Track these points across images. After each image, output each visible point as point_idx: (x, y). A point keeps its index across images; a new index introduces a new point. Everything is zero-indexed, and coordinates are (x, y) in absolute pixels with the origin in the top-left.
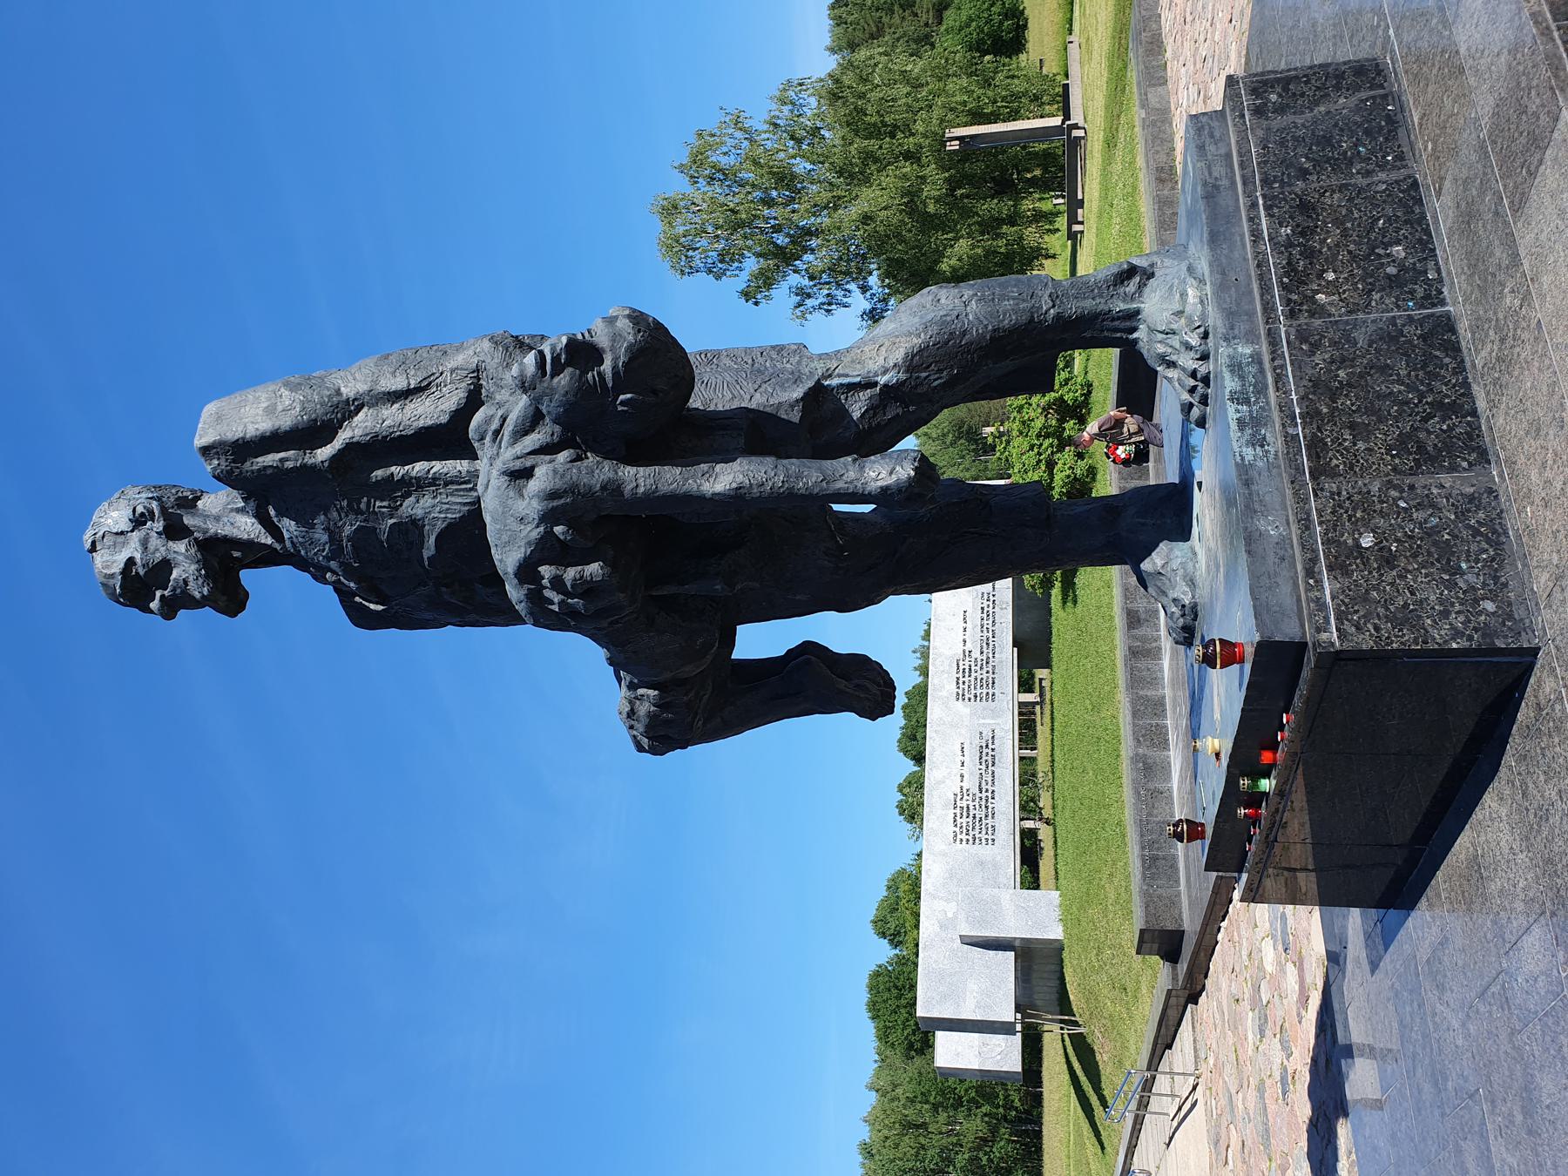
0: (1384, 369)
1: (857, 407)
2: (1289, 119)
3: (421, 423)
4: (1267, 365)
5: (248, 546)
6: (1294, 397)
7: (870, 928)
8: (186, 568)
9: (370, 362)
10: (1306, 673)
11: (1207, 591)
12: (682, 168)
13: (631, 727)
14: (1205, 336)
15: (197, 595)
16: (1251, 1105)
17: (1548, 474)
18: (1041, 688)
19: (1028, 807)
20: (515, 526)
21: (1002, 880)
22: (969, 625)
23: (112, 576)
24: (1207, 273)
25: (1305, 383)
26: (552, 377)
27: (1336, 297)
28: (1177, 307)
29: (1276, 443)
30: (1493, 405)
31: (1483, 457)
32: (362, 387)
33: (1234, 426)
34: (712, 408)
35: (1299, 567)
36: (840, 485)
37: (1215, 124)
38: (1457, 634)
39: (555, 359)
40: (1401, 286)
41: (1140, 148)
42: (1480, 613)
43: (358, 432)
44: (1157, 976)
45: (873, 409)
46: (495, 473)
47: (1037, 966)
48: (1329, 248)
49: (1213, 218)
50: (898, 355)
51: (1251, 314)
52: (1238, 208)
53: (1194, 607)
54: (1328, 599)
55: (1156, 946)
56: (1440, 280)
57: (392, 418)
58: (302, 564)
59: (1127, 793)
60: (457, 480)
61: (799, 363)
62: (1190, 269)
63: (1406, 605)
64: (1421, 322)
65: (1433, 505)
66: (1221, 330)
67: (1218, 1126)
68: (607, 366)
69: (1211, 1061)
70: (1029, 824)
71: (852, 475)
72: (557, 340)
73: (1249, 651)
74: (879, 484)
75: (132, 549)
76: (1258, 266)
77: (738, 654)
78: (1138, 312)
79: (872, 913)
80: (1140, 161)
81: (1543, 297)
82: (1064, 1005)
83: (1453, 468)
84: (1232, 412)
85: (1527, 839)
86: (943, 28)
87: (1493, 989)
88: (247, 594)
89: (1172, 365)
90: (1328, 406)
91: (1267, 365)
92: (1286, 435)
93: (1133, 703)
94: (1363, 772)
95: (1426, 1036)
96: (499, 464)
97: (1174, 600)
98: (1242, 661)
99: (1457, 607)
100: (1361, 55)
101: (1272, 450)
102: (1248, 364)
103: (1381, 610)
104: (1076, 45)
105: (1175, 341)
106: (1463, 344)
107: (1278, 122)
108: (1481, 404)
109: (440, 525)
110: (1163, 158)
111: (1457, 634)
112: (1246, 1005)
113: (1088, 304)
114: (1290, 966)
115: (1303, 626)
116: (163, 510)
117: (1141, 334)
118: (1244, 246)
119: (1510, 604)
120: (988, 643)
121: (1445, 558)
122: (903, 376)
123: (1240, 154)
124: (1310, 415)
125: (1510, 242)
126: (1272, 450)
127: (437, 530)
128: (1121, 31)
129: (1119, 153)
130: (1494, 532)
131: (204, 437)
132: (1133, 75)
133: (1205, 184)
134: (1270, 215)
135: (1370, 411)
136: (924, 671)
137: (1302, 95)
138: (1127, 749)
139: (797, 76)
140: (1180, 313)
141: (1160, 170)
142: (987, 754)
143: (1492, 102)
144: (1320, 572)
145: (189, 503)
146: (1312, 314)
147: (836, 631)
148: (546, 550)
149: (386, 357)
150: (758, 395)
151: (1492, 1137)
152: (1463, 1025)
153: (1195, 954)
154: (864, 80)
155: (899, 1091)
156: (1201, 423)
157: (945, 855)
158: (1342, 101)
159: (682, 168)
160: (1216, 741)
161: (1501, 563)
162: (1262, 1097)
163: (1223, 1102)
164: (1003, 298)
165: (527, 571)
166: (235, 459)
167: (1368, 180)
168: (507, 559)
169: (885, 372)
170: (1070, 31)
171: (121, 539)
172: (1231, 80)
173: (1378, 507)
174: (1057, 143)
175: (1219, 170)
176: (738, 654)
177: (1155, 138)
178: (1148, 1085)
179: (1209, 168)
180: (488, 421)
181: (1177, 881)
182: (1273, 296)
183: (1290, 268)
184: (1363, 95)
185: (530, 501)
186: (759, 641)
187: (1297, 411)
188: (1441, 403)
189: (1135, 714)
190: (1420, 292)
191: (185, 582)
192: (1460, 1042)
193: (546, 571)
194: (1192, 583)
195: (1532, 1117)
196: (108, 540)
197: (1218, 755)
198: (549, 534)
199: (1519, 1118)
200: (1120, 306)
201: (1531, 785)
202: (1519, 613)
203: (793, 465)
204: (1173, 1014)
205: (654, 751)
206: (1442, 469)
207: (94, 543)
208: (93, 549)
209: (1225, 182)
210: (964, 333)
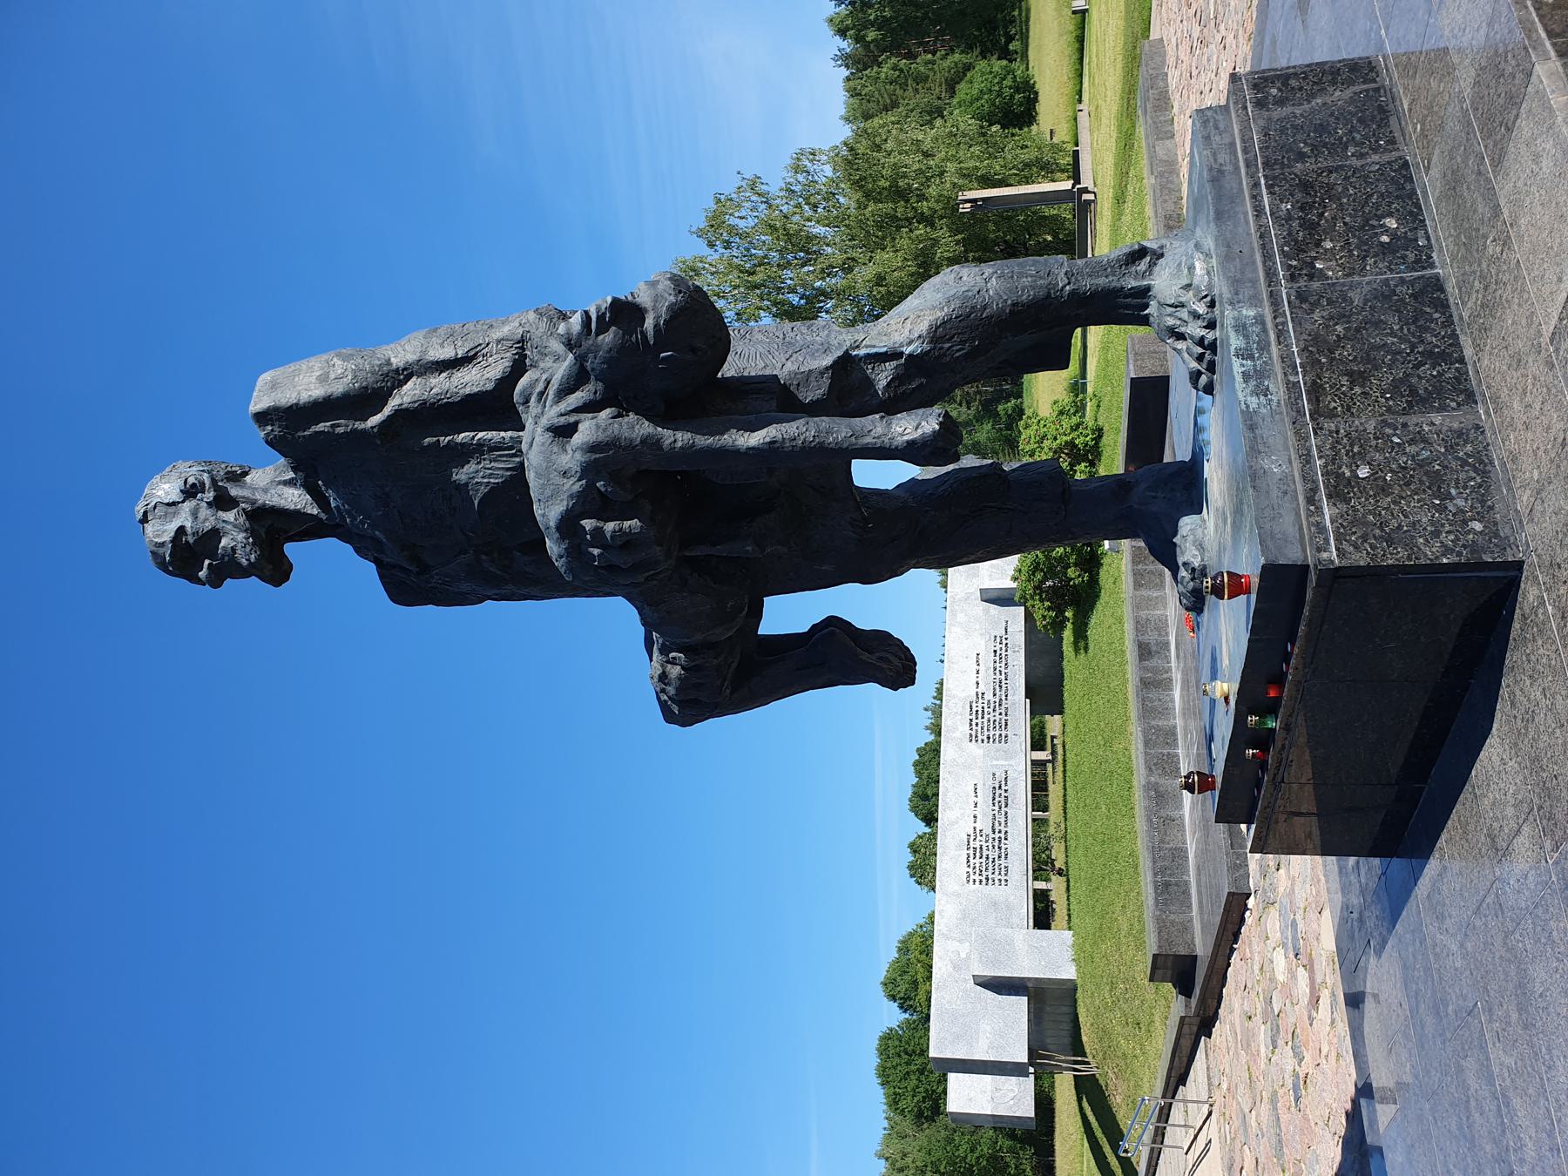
0: (1377, 324)
1: (882, 377)
2: (1288, 110)
3: (468, 391)
4: (1270, 325)
5: (297, 515)
6: (1295, 349)
7: (880, 992)
8: (234, 539)
9: (420, 334)
10: (1309, 595)
11: (1214, 553)
12: (700, 233)
13: (663, 691)
14: (1212, 305)
15: (244, 562)
16: (1264, 1119)
17: (1529, 399)
18: (1053, 746)
19: (1042, 865)
20: (559, 480)
21: (1015, 920)
22: (982, 668)
23: (162, 544)
26: (597, 335)
28: (1186, 282)
30: (1478, 348)
31: (1470, 397)
32: (411, 358)
33: (1239, 378)
35: (1301, 499)
36: (868, 440)
37: (1220, 117)
38: (1447, 550)
39: (600, 317)
40: (1394, 252)
41: (1149, 199)
42: (1469, 532)
43: (407, 399)
44: (1170, 1007)
46: (539, 430)
47: (1052, 1009)
49: (1218, 198)
50: (923, 327)
51: (1254, 282)
52: (1242, 190)
54: (1328, 523)
55: (1169, 973)
56: (1430, 247)
57: (440, 385)
58: (346, 536)
59: (1140, 824)
60: (499, 447)
62: (1197, 246)
63: (1400, 527)
64: (1412, 282)
65: (1425, 441)
66: (1227, 295)
67: (1232, 1150)
68: (649, 323)
69: (1224, 1086)
70: (1041, 885)
71: (879, 430)
72: (597, 302)
73: (1255, 581)
75: (183, 518)
77: (764, 629)
78: (1148, 289)
79: (882, 974)
80: (1149, 211)
81: (1520, 237)
82: (1077, 1048)
83: (1443, 408)
84: (1237, 367)
85: (1516, 744)
86: (955, 101)
87: (1488, 900)
88: (291, 566)
91: (1270, 325)
92: (1288, 382)
93: (1145, 733)
94: (1365, 718)
95: (1427, 969)
96: (544, 421)
97: (1185, 564)
98: (1248, 592)
99: (1447, 528)
100: (1355, 55)
101: (1275, 399)
103: (1378, 532)
104: (1085, 113)
105: (1184, 314)
106: (1451, 300)
107: (1278, 113)
108: (1468, 352)
109: (483, 490)
110: (1170, 206)
111: (1447, 550)
112: (1258, 1019)
113: (1102, 281)
114: (1301, 969)
115: (1304, 550)
116: (214, 481)
118: (1247, 222)
119: (1496, 524)
121: (1436, 484)
122: (926, 347)
123: (1243, 141)
124: (1311, 364)
125: (1490, 195)
126: (1275, 399)
128: (1128, 112)
129: (1128, 207)
130: (1481, 462)
131: (259, 403)
132: (1141, 131)
133: (1211, 169)
134: (1271, 193)
135: (1368, 359)
136: (937, 729)
137: (1301, 89)
138: (1139, 778)
139: (807, 145)
140: (1188, 287)
141: (1168, 218)
142: (1000, 795)
143: (1473, 73)
144: (1320, 500)
145: (237, 477)
147: (862, 605)
148: (588, 503)
149: (435, 330)
150: (789, 364)
151: (1490, 1045)
152: (1462, 945)
153: (1208, 978)
154: (878, 148)
155: (909, 1160)
156: (1209, 389)
157: (958, 895)
158: (1338, 93)
159: (700, 233)
160: (1225, 686)
161: (1488, 489)
162: (1275, 1108)
163: (1237, 1123)
164: (1021, 275)
165: (568, 526)
166: (289, 428)
167: (1363, 162)
168: (548, 512)
170: (1080, 101)
172: (1234, 78)
174: (1065, 211)
175: (1223, 157)
176: (764, 629)
177: (1163, 187)
178: (1164, 1114)
179: (1214, 155)
181: (1190, 907)
183: (1290, 239)
184: (1357, 88)
185: (571, 457)
186: (788, 614)
188: (1431, 352)
189: (1147, 743)
190: (1411, 256)
192: (1458, 965)
193: (588, 524)
194: (1201, 547)
195: (1527, 1011)
196: (160, 511)
197: (1227, 699)
198: (589, 488)
199: (1514, 1016)
200: (1132, 283)
201: (1518, 693)
202: (1504, 531)
204: (1186, 1044)
205: (685, 723)
206: (1433, 409)
207: (145, 513)
208: (144, 519)
209: (1229, 168)
210: (985, 307)
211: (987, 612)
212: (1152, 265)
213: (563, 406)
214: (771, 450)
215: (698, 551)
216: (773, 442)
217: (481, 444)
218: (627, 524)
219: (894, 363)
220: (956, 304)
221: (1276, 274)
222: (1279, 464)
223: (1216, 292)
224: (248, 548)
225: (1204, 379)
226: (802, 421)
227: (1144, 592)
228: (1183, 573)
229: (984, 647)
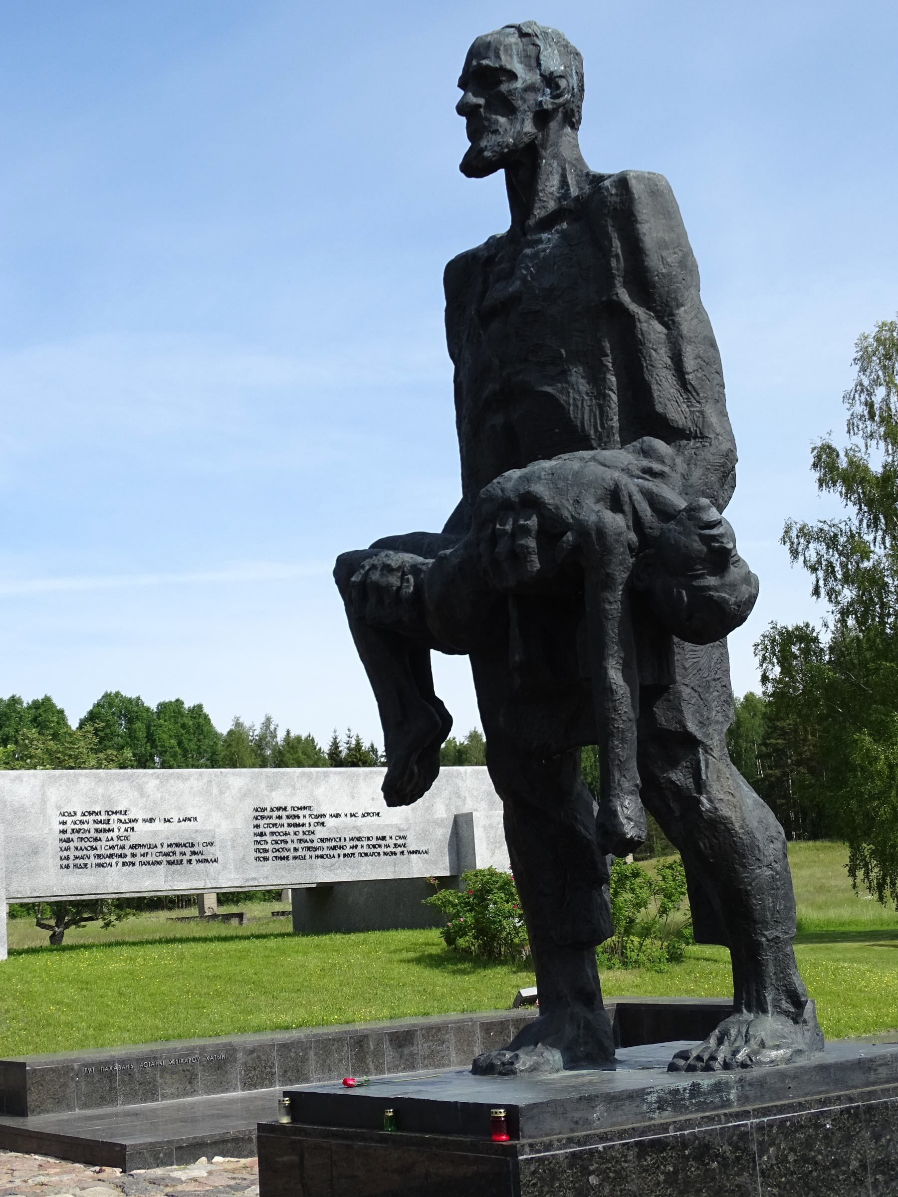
1: (679, 777)
3: (654, 387)
6: (697, 1130)
14: (744, 1065)
15: (483, 143)
20: (572, 494)
22: (360, 821)
23: (498, 57)
25: (707, 1138)
27: (774, 1162)
28: (769, 1043)
29: (659, 1118)
34: (676, 650)
36: (617, 775)
39: (714, 538)
45: (677, 790)
46: (617, 474)
48: (814, 1157)
50: (725, 811)
53: (513, 1072)
61: (717, 722)
62: (799, 1052)
68: (712, 581)
71: (626, 785)
74: (619, 808)
76: (800, 1103)
78: (765, 1011)
89: (720, 1042)
90: (690, 1154)
92: (668, 1124)
93: (297, 1044)
96: (624, 479)
97: (517, 1056)
101: (656, 1116)
102: (721, 1097)
103: (546, 1189)
109: (562, 398)
113: (771, 969)
117: (747, 1015)
120: (336, 847)
124: (684, 1143)
127: (558, 395)
134: (842, 1112)
140: (763, 1045)
142: (183, 853)
146: (760, 1144)
148: (552, 526)
150: (688, 690)
165: (529, 502)
169: (710, 800)
171: (534, 63)
173: (618, 1188)
176: (435, 656)
179: (886, 1064)
180: (661, 460)
181: (85, 1106)
182: (775, 1115)
185: (594, 511)
186: (453, 679)
187: (686, 1132)
189: (285, 1047)
191: (496, 132)
193: (533, 522)
194: (534, 1069)
198: (567, 527)
203: (632, 735)
209: (872, 1077)
210: (744, 866)
211: (439, 823)
212: (787, 1013)
213: (638, 497)
214: (608, 690)
216: (612, 691)
217: (605, 396)
218: (535, 558)
219: (692, 786)
220: (746, 840)
221: (764, 1115)
222: (600, 1118)
223: (755, 1068)
224: (497, 149)
225: (681, 1062)
226: (632, 716)
227: (479, 1034)
228: (508, 1055)
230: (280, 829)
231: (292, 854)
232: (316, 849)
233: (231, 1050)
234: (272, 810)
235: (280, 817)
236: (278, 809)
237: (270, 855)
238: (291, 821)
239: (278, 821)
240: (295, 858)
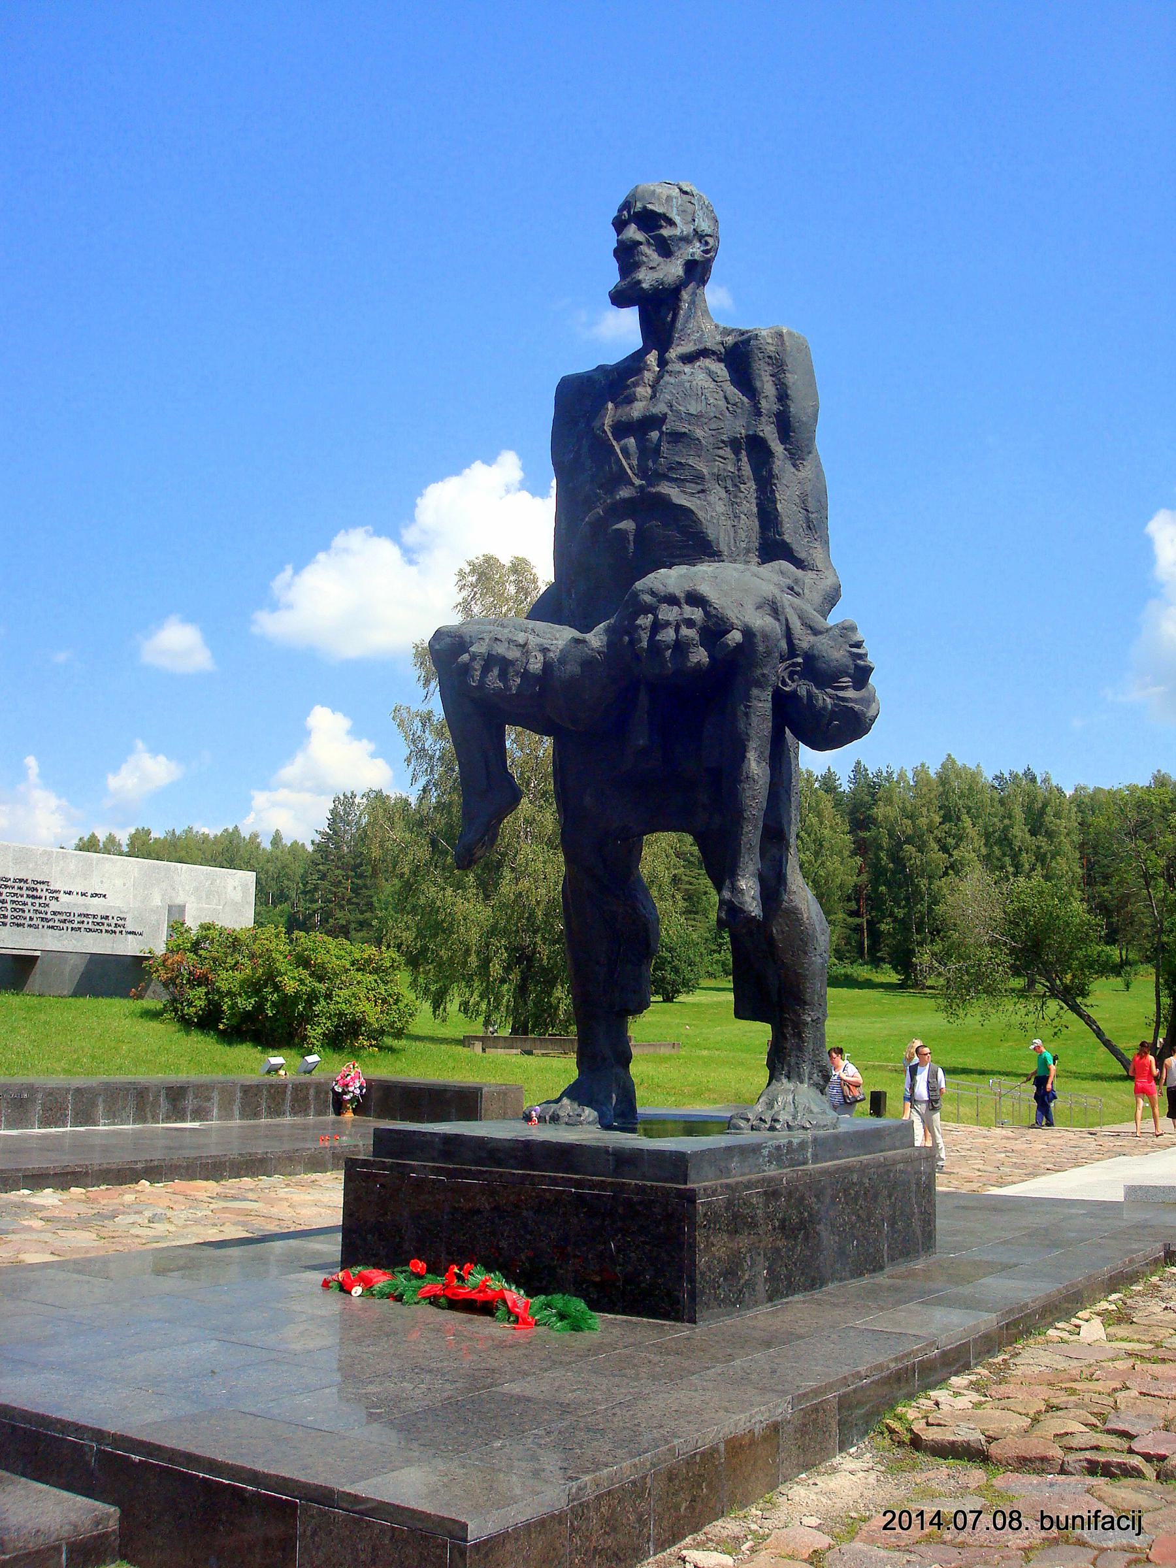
24: (840, 1130)
68: (850, 693)
200: (806, 1068)
210: (806, 953)
212: (816, 1085)
215: (643, 698)
229: (113, 904)
230: (20, 899)
231: (27, 922)
232: (48, 920)
233: (32, 1089)
234: (15, 881)
235: (20, 888)
236: (21, 880)
237: (8, 921)
238: (30, 893)
239: (18, 891)
240: (30, 926)
